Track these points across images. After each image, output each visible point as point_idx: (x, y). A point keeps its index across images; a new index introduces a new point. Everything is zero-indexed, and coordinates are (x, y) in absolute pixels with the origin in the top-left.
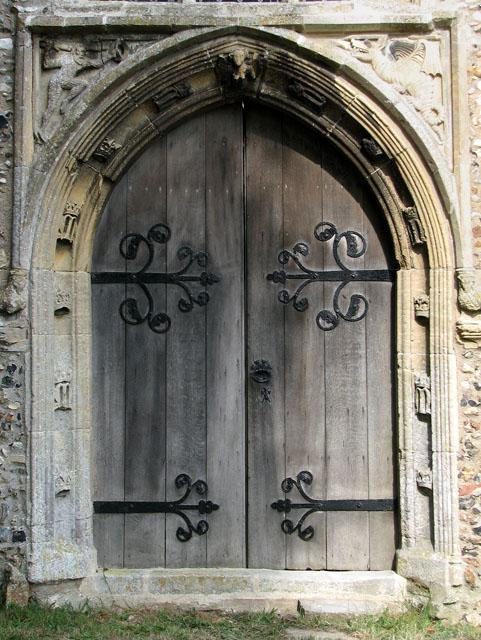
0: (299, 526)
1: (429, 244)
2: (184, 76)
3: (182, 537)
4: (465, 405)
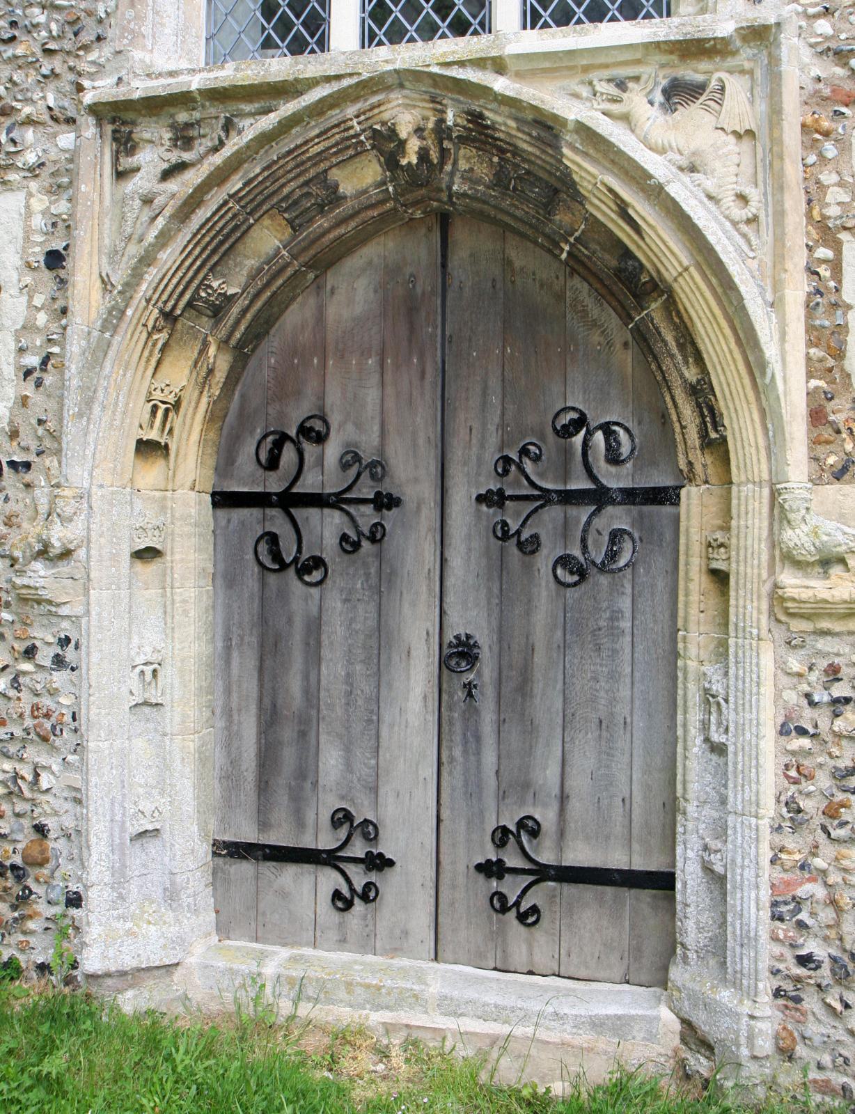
0: (517, 904)
1: (730, 439)
2: (323, 166)
3: (340, 904)
4: (788, 733)
